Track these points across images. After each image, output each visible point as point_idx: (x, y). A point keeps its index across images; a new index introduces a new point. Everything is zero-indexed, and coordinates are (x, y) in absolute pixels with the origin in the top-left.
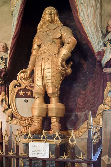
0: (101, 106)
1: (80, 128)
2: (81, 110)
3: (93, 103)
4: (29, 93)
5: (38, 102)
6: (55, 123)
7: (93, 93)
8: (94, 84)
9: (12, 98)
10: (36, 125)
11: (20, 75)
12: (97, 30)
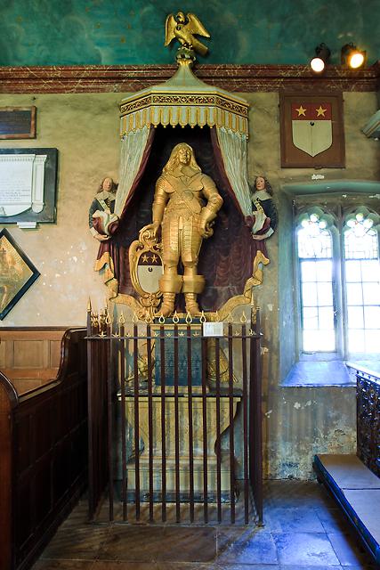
0: (250, 280)
1: (222, 310)
2: (221, 283)
3: (239, 275)
4: (154, 258)
5: (170, 273)
6: (191, 302)
7: (238, 262)
8: (240, 249)
9: (134, 266)
10: (168, 304)
11: (144, 232)
12: (245, 185)
